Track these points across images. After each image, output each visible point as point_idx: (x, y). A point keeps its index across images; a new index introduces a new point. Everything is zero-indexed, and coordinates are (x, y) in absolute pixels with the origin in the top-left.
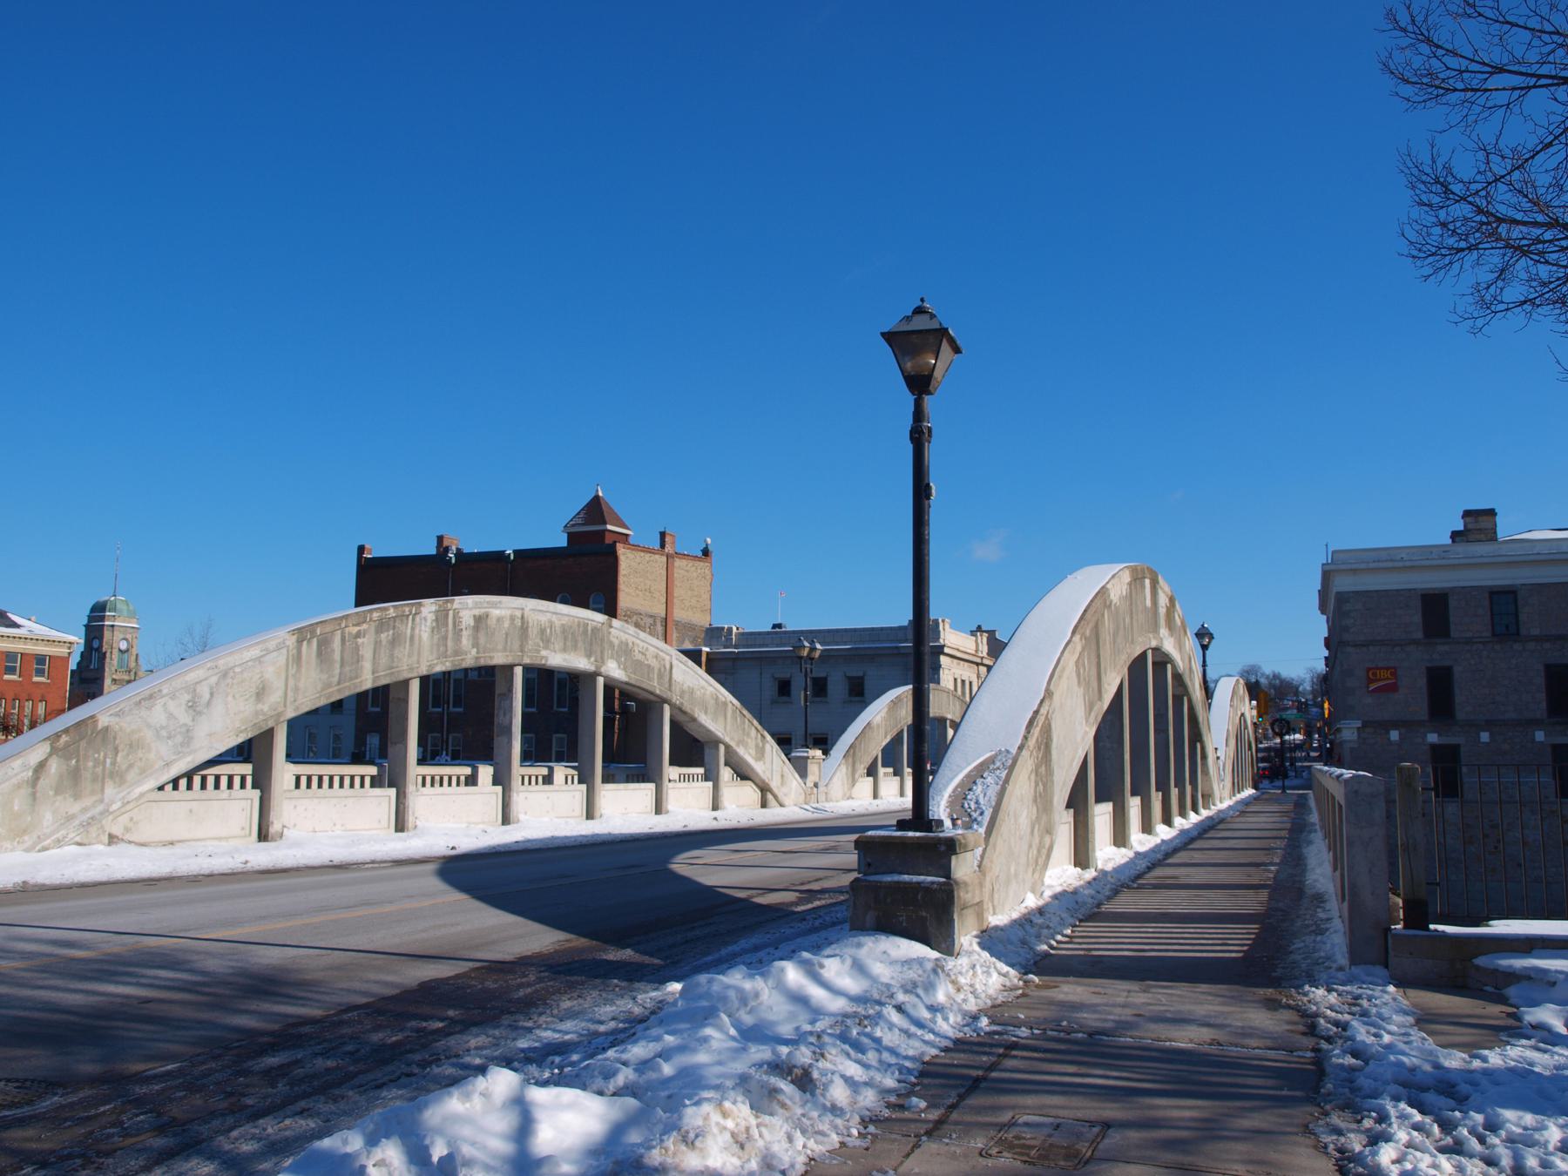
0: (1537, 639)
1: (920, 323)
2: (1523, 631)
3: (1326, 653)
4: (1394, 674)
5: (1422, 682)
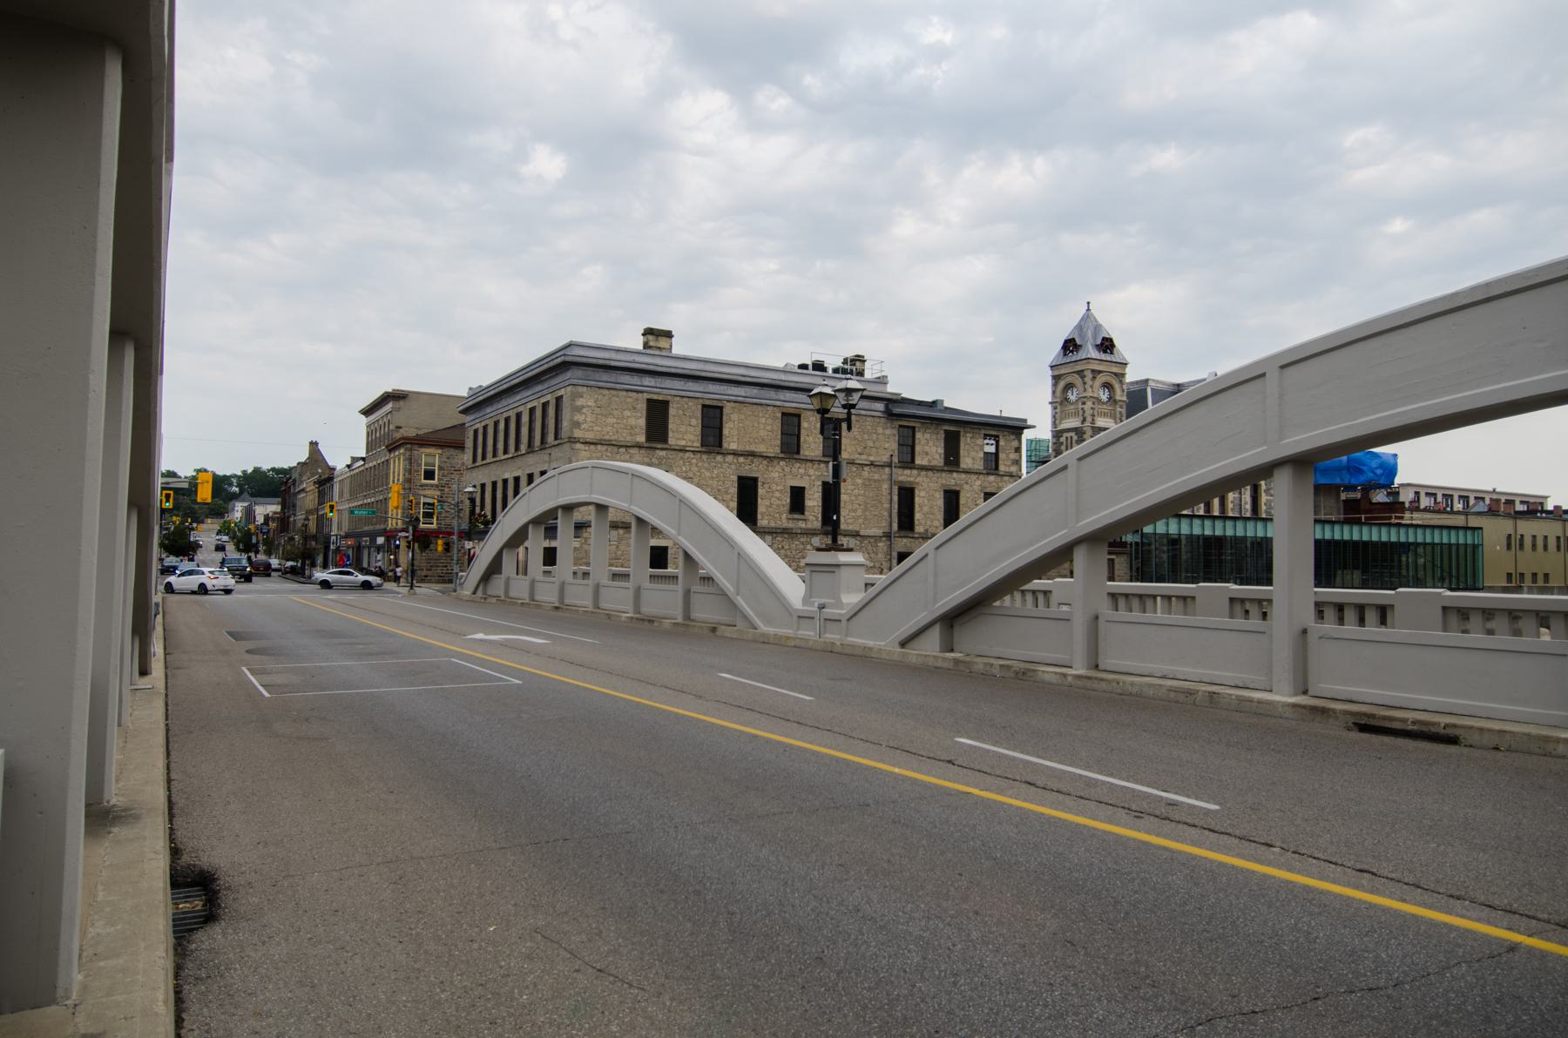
0: (735, 454)
2: (725, 445)
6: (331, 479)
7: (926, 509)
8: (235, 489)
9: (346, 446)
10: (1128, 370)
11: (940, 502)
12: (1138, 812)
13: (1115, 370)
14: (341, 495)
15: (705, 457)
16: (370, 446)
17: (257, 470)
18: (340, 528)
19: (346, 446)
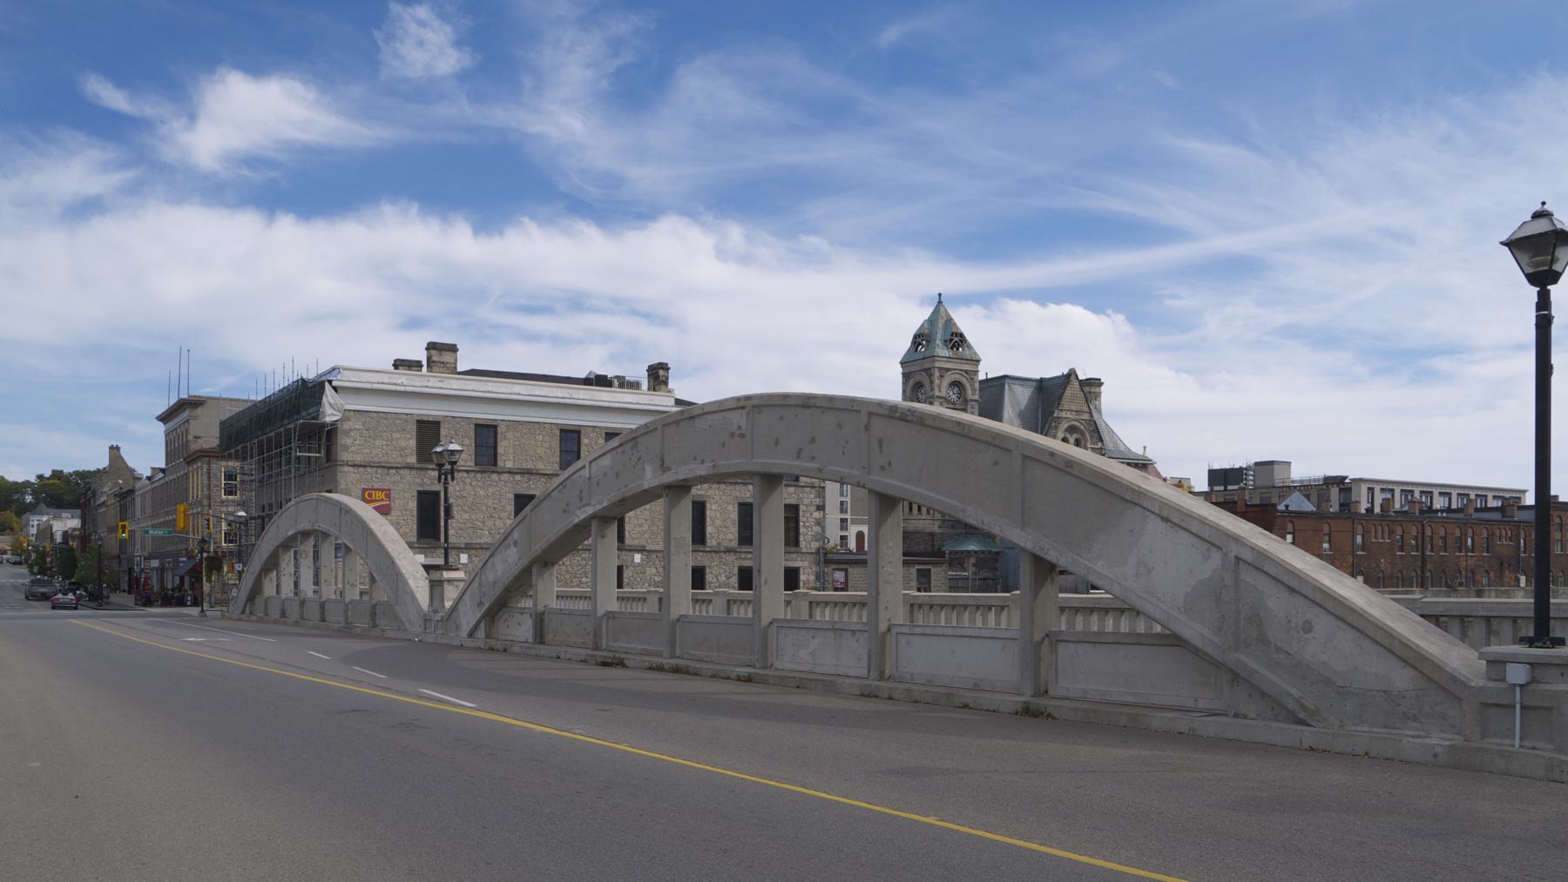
0: (511, 472)
1: (1542, 226)
2: (500, 463)
3: (1360, 578)
4: (388, 496)
5: (413, 505)
6: (132, 492)
7: (718, 522)
8: (29, 499)
9: (147, 454)
10: (981, 367)
11: (734, 515)
12: (448, 703)
13: (966, 367)
14: (143, 511)
15: (479, 476)
16: (170, 456)
17: (57, 474)
18: (143, 547)
19: (147, 454)
